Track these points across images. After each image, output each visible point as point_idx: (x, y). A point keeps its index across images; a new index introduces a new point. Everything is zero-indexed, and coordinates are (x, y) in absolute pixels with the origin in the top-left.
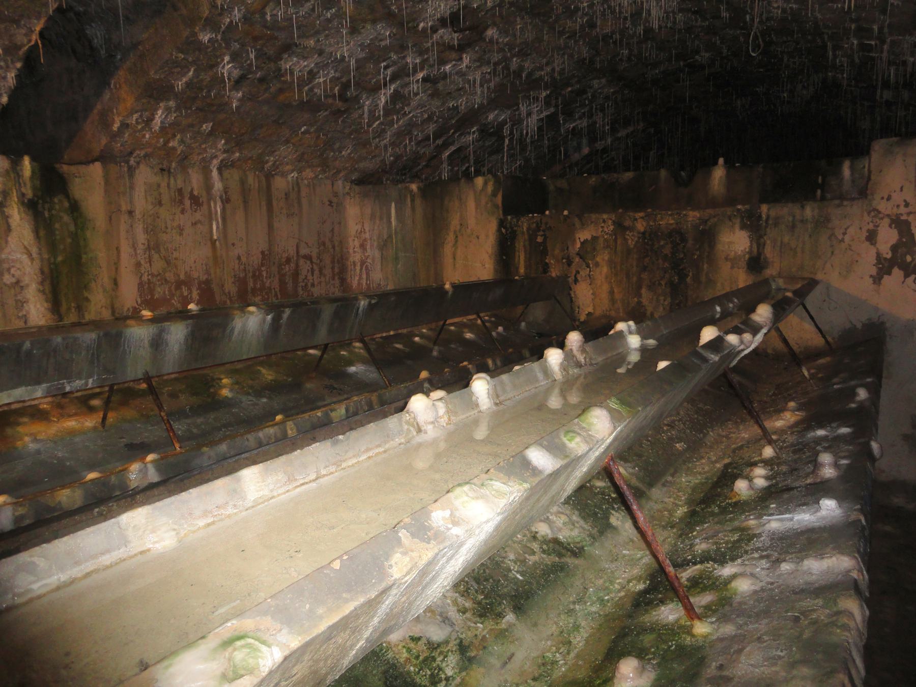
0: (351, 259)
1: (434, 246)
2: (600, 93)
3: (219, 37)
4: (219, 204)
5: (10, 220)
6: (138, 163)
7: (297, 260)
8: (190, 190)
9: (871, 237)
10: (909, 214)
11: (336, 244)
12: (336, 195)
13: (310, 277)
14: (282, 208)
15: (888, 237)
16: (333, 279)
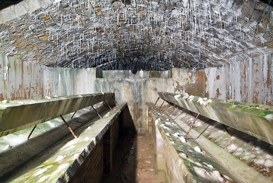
0: (45, 89)
1: (74, 85)
7: (30, 88)
9: (173, 85)
12: (41, 69)
13: (33, 94)
14: (26, 71)
15: (176, 85)
16: (40, 95)
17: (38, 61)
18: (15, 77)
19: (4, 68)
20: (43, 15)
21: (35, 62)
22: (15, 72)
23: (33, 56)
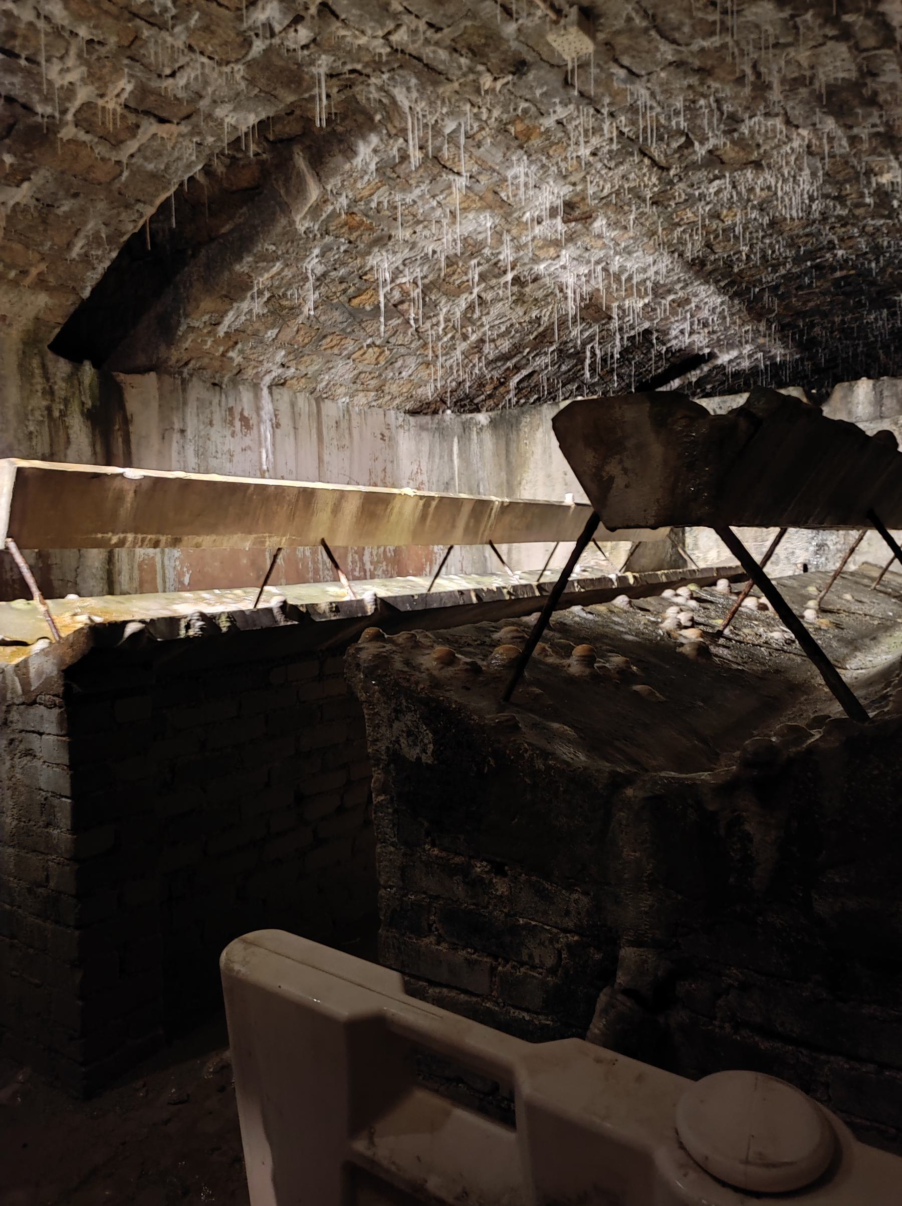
2: (706, 303)
3: (316, 227)
4: (269, 428)
5: (70, 431)
6: (191, 375)
8: (240, 410)
14: (332, 439)
17: (373, 394)
18: (296, 459)
19: (259, 431)
20: (334, 215)
21: (361, 399)
22: (296, 443)
23: (351, 376)
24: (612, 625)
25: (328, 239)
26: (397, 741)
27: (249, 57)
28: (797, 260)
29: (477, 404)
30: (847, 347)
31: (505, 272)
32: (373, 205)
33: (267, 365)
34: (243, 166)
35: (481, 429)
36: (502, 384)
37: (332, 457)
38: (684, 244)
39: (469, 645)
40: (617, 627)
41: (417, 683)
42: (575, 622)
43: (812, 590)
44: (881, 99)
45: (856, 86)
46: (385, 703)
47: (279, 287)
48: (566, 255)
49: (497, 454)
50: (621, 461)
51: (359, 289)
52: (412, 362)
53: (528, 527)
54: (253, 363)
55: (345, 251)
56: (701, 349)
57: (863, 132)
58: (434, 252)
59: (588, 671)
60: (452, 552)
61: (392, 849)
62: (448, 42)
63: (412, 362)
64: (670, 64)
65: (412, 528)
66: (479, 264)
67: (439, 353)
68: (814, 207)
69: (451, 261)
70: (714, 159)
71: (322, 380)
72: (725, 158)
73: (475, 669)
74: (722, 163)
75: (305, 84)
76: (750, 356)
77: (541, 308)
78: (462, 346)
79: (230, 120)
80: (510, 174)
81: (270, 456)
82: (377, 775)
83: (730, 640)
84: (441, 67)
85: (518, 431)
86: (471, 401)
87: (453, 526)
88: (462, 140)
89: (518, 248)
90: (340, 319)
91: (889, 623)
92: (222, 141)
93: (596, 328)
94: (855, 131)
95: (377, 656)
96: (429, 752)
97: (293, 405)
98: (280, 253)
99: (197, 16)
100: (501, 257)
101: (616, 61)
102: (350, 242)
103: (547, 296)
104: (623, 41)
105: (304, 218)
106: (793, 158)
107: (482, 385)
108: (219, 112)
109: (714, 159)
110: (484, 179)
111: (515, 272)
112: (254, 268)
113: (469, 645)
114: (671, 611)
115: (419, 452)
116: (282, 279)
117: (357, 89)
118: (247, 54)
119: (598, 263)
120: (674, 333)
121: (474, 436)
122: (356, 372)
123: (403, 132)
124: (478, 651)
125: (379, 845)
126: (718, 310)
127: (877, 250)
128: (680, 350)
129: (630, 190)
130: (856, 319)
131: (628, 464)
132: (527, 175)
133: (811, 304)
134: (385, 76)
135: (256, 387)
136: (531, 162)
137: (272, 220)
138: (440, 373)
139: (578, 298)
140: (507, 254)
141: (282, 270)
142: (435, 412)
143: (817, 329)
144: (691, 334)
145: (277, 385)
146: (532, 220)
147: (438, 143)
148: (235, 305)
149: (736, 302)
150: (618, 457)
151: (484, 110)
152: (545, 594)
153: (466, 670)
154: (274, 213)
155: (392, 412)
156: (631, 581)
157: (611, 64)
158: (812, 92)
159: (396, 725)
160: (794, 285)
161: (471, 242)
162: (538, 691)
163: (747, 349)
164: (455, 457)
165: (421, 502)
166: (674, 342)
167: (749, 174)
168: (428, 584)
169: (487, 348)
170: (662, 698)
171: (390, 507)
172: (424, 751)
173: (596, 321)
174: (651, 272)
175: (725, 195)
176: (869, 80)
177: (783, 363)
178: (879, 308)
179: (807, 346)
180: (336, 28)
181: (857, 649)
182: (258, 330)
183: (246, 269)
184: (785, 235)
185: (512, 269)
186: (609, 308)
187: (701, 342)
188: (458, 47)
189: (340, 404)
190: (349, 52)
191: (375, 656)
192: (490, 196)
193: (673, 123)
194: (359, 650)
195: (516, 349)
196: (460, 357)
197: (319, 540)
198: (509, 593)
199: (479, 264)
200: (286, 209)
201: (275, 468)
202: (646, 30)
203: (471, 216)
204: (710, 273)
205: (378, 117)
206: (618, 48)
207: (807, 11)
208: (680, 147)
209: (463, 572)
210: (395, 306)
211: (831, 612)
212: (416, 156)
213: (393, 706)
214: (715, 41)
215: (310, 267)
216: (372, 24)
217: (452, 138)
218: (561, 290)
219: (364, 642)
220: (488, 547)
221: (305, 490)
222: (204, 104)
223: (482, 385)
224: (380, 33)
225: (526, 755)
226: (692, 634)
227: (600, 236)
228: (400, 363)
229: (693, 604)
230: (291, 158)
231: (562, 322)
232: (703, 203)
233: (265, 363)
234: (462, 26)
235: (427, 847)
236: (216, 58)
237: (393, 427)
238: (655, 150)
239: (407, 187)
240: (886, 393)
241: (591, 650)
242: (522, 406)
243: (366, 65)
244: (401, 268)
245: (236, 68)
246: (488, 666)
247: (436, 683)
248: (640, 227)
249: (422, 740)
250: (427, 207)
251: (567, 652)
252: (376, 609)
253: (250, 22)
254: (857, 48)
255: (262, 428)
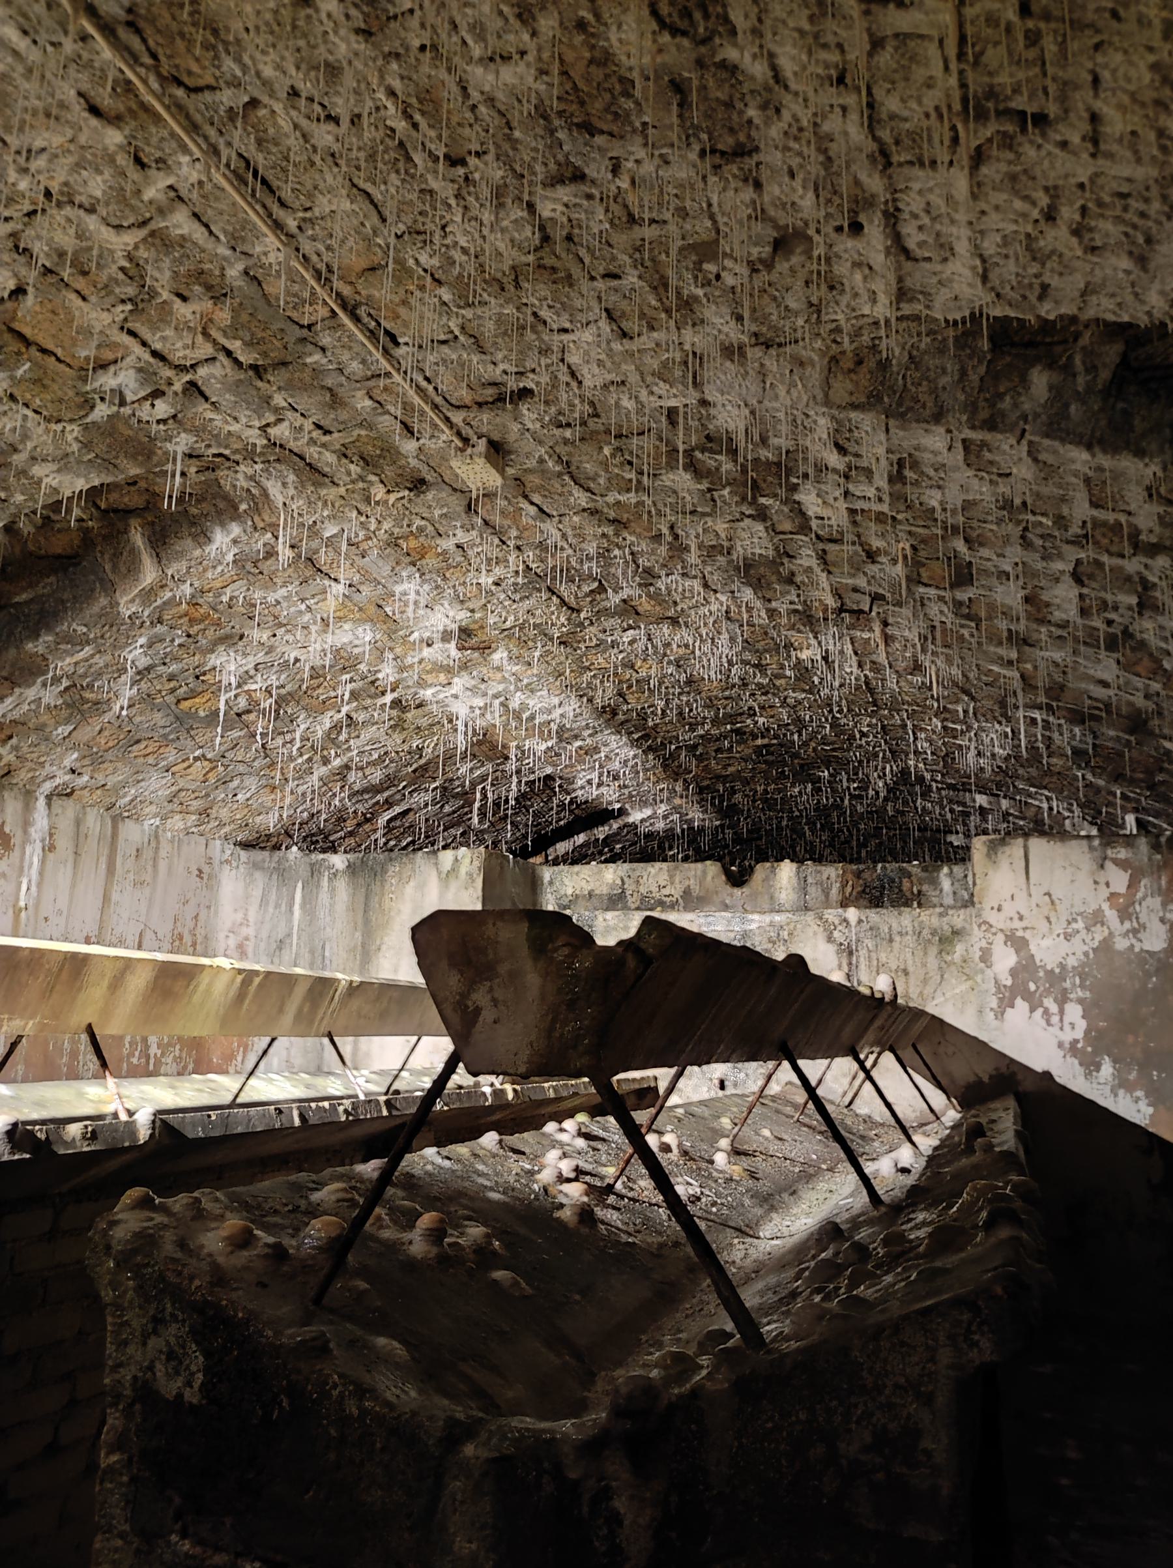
3: (146, 613)
4: (39, 851)
10: (1025, 929)
11: (200, 939)
12: (210, 861)
18: (71, 895)
19: (24, 853)
20: (172, 602)
22: (75, 874)
24: (475, 1177)
25: (160, 629)
26: (151, 1368)
27: (88, 420)
28: (715, 722)
29: (333, 842)
30: (770, 818)
31: (383, 693)
32: (225, 599)
33: (48, 769)
34: (59, 531)
35: (335, 875)
36: (367, 820)
37: (126, 899)
38: (595, 689)
39: (276, 1212)
40: (481, 1180)
41: (192, 1278)
42: (427, 1173)
43: (726, 1122)
44: (798, 579)
45: (775, 564)
46: (141, 1307)
47: (85, 676)
48: (460, 683)
49: (352, 909)
50: (491, 990)
51: (192, 690)
52: (252, 783)
53: (383, 1015)
54: (29, 764)
55: (180, 645)
56: (610, 803)
57: (782, 606)
58: (297, 660)
59: (435, 1250)
60: (276, 1043)
61: (119, 1543)
62: (338, 447)
63: (252, 783)
64: (584, 510)
65: (222, 1011)
66: (352, 680)
67: (290, 776)
68: (733, 671)
69: (316, 673)
70: (628, 609)
71: (124, 796)
72: (640, 609)
73: (279, 1253)
74: (637, 613)
75: (155, 459)
76: (665, 817)
77: (424, 738)
78: (321, 771)
79: (52, 481)
80: (398, 589)
81: (34, 888)
82: (114, 1420)
83: (622, 1197)
84: (327, 469)
85: (383, 881)
86: (326, 837)
87: (281, 1010)
88: (344, 547)
89: (402, 670)
90: (162, 723)
91: (811, 1170)
92: (36, 502)
93: (489, 767)
94: (774, 604)
95: (138, 1235)
96: (197, 1385)
97: (78, 823)
98: (92, 636)
99: (27, 366)
100: (380, 676)
101: (526, 497)
102: (189, 636)
103: (432, 725)
104: (533, 480)
105: (132, 601)
106: (711, 620)
107: (341, 820)
108: (37, 470)
109: (628, 609)
110: (366, 590)
111: (395, 695)
112: (54, 649)
113: (276, 1212)
114: (552, 1155)
115: (247, 897)
116: (90, 666)
117: (221, 473)
118: (87, 415)
119: (496, 696)
120: (580, 783)
121: (325, 882)
122: (174, 788)
123: (273, 528)
124: (286, 1222)
125: (99, 1537)
126: (630, 764)
127: (800, 724)
128: (586, 802)
129: (536, 626)
130: (779, 791)
131: (499, 994)
132: (418, 593)
133: (731, 769)
134: (258, 467)
135: (28, 795)
136: (424, 582)
137: (90, 596)
138: (288, 801)
139: (470, 733)
140: (387, 673)
141: (92, 656)
142: (277, 847)
143: (738, 797)
144: (599, 785)
145: (59, 795)
146: (422, 641)
147: (315, 544)
148: (17, 690)
149: (651, 757)
150: (488, 984)
151: (373, 520)
152: (395, 1113)
153: (266, 1256)
154: (93, 590)
155: (218, 842)
156: (510, 1096)
157: (520, 499)
158: (730, 562)
159: (153, 1342)
160: (712, 747)
161: (343, 653)
162: (363, 1285)
163: (662, 809)
164: (297, 908)
165: (240, 978)
166: (579, 793)
167: (666, 629)
168: (238, 1086)
169: (352, 777)
170: (529, 1290)
171: (194, 983)
172: (189, 1384)
173: (490, 759)
174: (556, 714)
175: (639, 646)
176: (786, 560)
177: (702, 829)
178: (804, 782)
179: (728, 812)
180: (202, 407)
181: (773, 1208)
182: (45, 725)
183: (41, 649)
184: (703, 695)
185: (393, 690)
186: (504, 746)
187: (610, 795)
188: (349, 453)
189: (146, 827)
190: (217, 436)
191: (136, 1235)
192: (373, 609)
193: (586, 567)
194: (113, 1224)
195: (390, 781)
196: (317, 784)
197: (84, 1025)
198: (346, 1111)
199: (352, 680)
200: (110, 588)
201: (37, 905)
202: (560, 475)
203: (347, 627)
204: (622, 723)
205: (243, 507)
206: (528, 485)
207: (724, 487)
208: (592, 591)
209: (290, 1069)
210: (239, 715)
211: (746, 1154)
212: (285, 553)
213: (152, 1312)
214: (631, 498)
215: (130, 657)
216: (248, 413)
217: (330, 542)
218: (450, 721)
219: (122, 1211)
220: (326, 1041)
221: (74, 956)
222: (18, 459)
223: (341, 820)
224: (257, 424)
225: (335, 1393)
226: (574, 1192)
227: (499, 669)
228: (236, 783)
229: (581, 1143)
230: (126, 532)
231: (449, 757)
232: (616, 650)
233: (47, 765)
234: (356, 433)
235: (174, 1538)
236: (45, 413)
237: (216, 862)
238: (563, 589)
239: (271, 584)
240: (810, 880)
241: (442, 1221)
242: (391, 850)
243: (236, 451)
244: (252, 672)
245: (68, 428)
246: (298, 1248)
247: (219, 1277)
248: (544, 666)
249: (188, 1368)
250: (292, 609)
251: (408, 1220)
252: (152, 1135)
253: (96, 385)
254: (773, 530)
255: (28, 850)
